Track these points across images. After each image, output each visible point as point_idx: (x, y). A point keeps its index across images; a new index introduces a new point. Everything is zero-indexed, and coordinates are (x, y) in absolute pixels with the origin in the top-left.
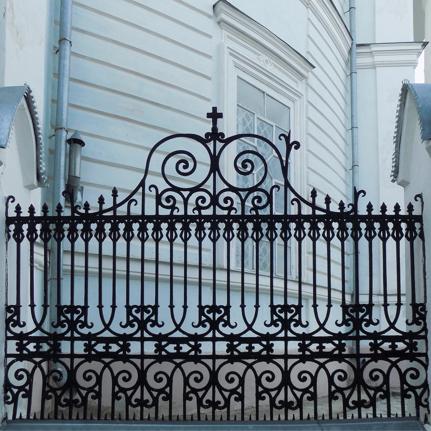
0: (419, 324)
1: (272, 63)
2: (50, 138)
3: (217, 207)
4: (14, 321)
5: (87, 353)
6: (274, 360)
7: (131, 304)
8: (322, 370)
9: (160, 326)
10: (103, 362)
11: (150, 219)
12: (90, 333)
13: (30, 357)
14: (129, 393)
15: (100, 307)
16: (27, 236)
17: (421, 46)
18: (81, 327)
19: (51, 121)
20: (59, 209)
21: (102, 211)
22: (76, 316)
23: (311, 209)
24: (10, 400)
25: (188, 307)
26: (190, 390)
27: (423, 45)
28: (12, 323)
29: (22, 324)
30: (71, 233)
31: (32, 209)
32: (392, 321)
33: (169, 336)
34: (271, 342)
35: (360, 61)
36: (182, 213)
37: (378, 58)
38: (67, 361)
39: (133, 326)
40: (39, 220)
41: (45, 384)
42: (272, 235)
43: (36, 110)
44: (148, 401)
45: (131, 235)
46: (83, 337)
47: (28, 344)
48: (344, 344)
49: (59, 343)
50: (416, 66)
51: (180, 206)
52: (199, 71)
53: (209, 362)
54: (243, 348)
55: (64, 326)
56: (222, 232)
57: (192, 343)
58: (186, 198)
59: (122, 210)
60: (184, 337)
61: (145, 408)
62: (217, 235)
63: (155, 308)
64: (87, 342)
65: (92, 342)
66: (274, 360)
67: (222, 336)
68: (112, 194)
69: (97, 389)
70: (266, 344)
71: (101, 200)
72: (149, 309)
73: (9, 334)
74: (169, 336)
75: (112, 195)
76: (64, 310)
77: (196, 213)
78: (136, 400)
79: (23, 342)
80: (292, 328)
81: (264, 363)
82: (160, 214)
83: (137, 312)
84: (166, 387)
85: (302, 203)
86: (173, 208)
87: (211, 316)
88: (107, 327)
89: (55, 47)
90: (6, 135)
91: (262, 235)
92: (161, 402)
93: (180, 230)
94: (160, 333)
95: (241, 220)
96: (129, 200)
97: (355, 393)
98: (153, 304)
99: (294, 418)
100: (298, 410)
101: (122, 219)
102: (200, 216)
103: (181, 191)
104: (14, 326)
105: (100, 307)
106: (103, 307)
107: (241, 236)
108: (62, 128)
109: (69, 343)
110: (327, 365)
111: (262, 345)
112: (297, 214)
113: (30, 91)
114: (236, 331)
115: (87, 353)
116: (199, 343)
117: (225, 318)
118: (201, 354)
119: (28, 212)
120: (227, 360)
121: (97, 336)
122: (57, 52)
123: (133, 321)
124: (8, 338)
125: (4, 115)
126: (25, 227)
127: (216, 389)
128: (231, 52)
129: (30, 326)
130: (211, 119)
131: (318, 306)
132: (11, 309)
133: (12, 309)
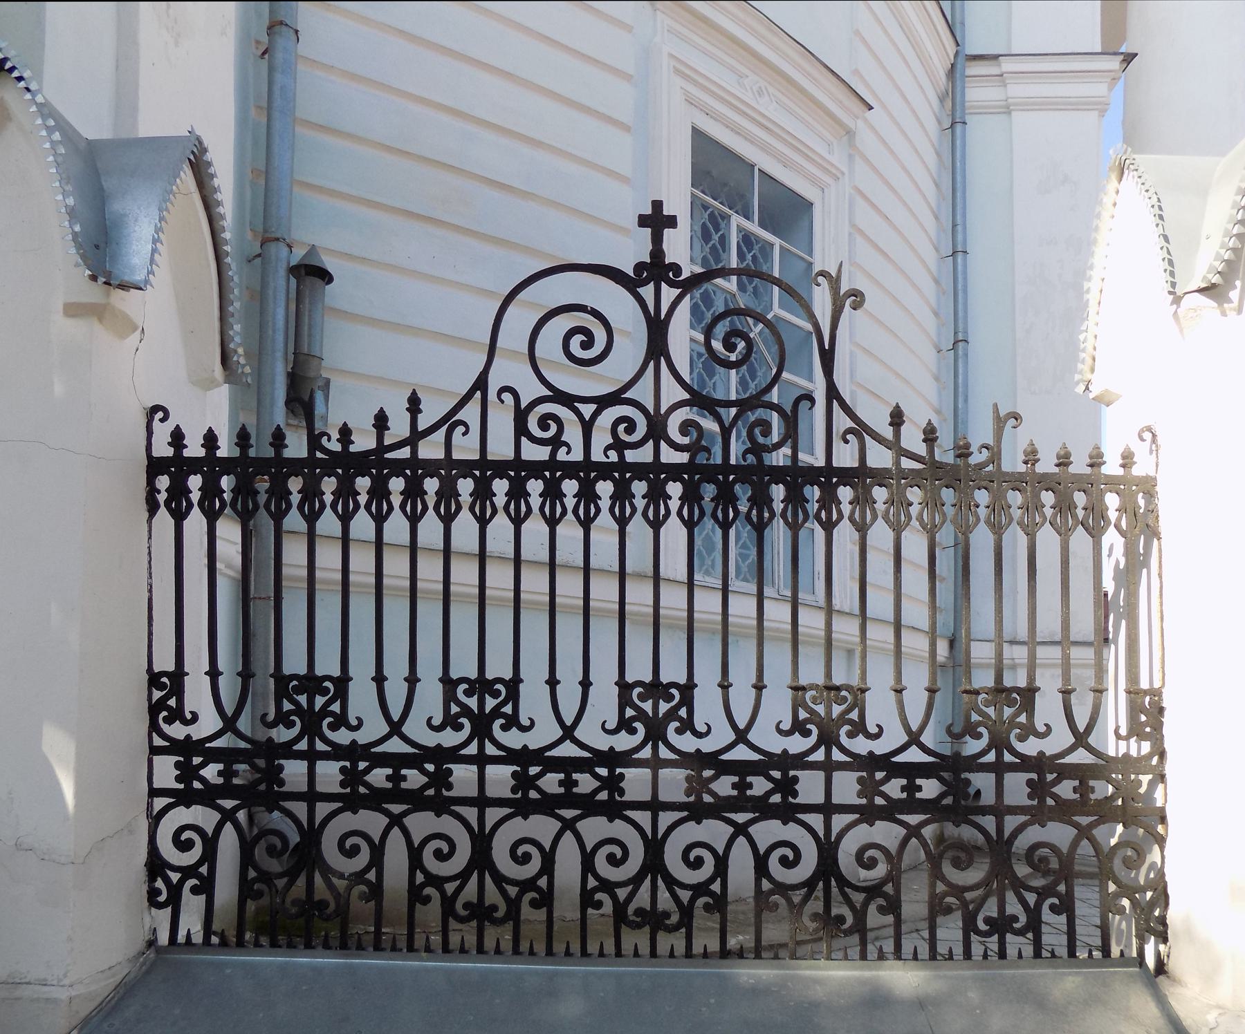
0: (1141, 737)
1: (773, 95)
2: (250, 261)
3: (663, 444)
4: (169, 708)
5: (348, 790)
6: (798, 816)
7: (630, 678)
8: (568, 835)
9: (524, 729)
10: (1076, 825)
11: (500, 468)
12: (188, 737)
13: (208, 796)
14: (450, 888)
15: (380, 679)
16: (201, 504)
17: (1118, 63)
18: (334, 727)
19: (251, 223)
20: (278, 439)
21: (381, 448)
22: (320, 701)
24: (162, 898)
25: (591, 684)
26: (598, 883)
27: (1124, 60)
28: (165, 713)
29: (189, 716)
31: (210, 440)
32: (396, 718)
33: (546, 754)
34: (792, 773)
35: (977, 94)
36: (577, 455)
37: (1017, 90)
38: (300, 809)
39: (458, 727)
40: (228, 465)
41: (247, 859)
42: (795, 515)
43: (219, 196)
44: (494, 908)
46: (337, 752)
47: (203, 765)
49: (279, 764)
50: (1106, 110)
51: (573, 434)
52: (602, 110)
53: (471, 814)
55: (978, 736)
56: (674, 504)
57: (603, 772)
58: (587, 420)
59: (431, 450)
60: (583, 757)
61: (1009, 937)
62: (662, 512)
63: (513, 685)
64: (348, 764)
65: (360, 763)
66: (798, 816)
67: (673, 756)
68: (408, 406)
69: (372, 876)
70: (779, 777)
71: (381, 422)
72: (499, 686)
73: (158, 742)
74: (546, 754)
75: (407, 409)
76: (290, 687)
77: (613, 456)
78: (467, 905)
79: (192, 760)
80: (844, 740)
81: (776, 823)
82: (664, 459)
83: (468, 693)
84: (539, 875)
86: (556, 442)
87: (647, 706)
88: (396, 728)
89: (258, 42)
90: (146, 257)
91: (702, 514)
92: (526, 911)
94: (525, 747)
95: (720, 477)
96: (450, 421)
97: (301, 882)
98: (508, 675)
100: (509, 926)
101: (431, 468)
102: (622, 465)
103: (575, 404)
104: (168, 721)
105: (380, 679)
106: (387, 679)
108: (277, 239)
109: (821, 775)
110: (408, 821)
111: (770, 779)
112: (856, 465)
113: (205, 150)
114: (708, 746)
115: (348, 790)
116: (618, 771)
117: (683, 712)
118: (623, 799)
119: (202, 446)
120: (686, 813)
121: (372, 750)
122: (264, 53)
123: (458, 715)
124: (154, 751)
125: (139, 208)
126: (195, 482)
127: (660, 882)
128: (678, 66)
129: (209, 723)
130: (648, 231)
132: (162, 680)
133: (164, 680)
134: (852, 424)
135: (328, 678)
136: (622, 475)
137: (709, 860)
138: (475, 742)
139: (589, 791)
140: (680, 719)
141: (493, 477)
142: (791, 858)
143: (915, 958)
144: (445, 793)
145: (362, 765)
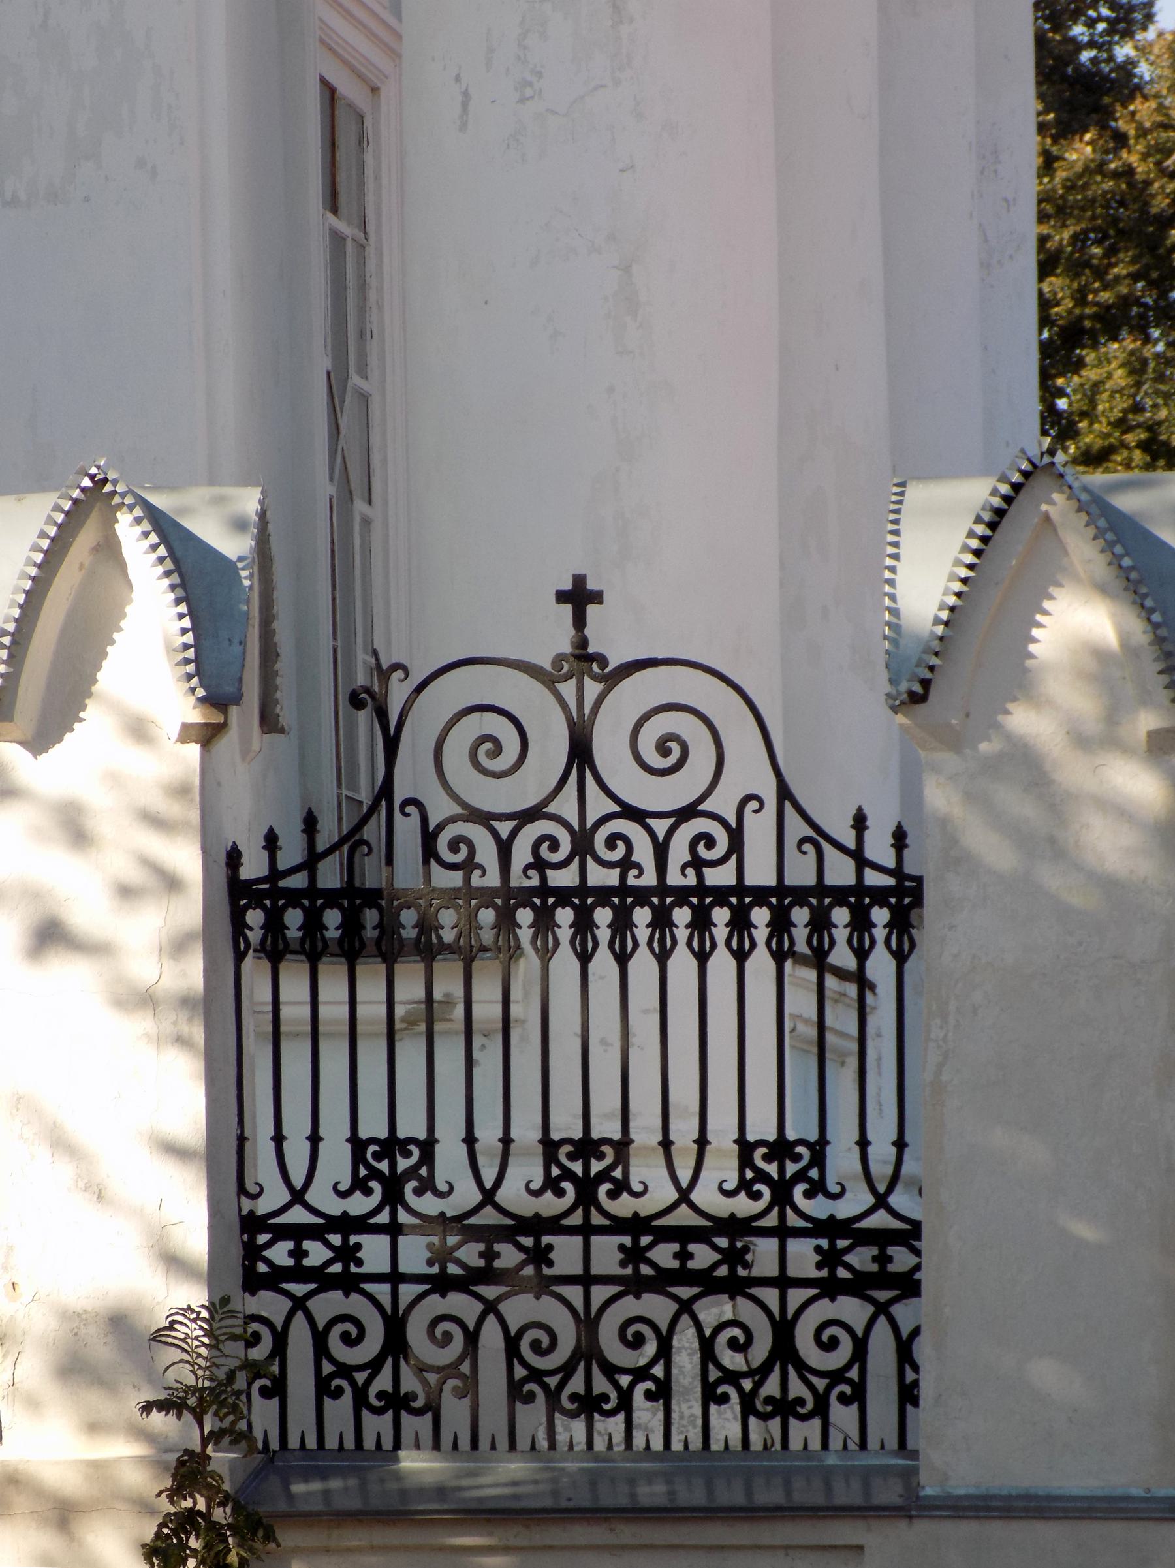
8: (882, 1321)
15: (279, 1139)
23: (850, 864)
30: (422, 934)
32: (684, 1185)
45: (357, 944)
48: (550, 1247)
53: (770, 1296)
54: (664, 1255)
72: (800, 1149)
77: (691, 880)
81: (338, 1294)
83: (571, 1157)
85: (828, 849)
86: (469, 865)
93: (648, 926)
99: (648, 1447)
100: (816, 1423)
102: (701, 889)
105: (279, 1139)
107: (656, 945)
121: (754, 1224)
127: (791, 1369)
130: (568, 609)
131: (694, 1141)
134: (811, 833)
135: (801, 1142)
136: (313, 902)
137: (458, 1340)
138: (387, 1209)
139: (906, 1269)
140: (420, 1178)
141: (751, 905)
142: (354, 1336)
143: (455, 1447)
144: (353, 1269)
145: (645, 1240)
